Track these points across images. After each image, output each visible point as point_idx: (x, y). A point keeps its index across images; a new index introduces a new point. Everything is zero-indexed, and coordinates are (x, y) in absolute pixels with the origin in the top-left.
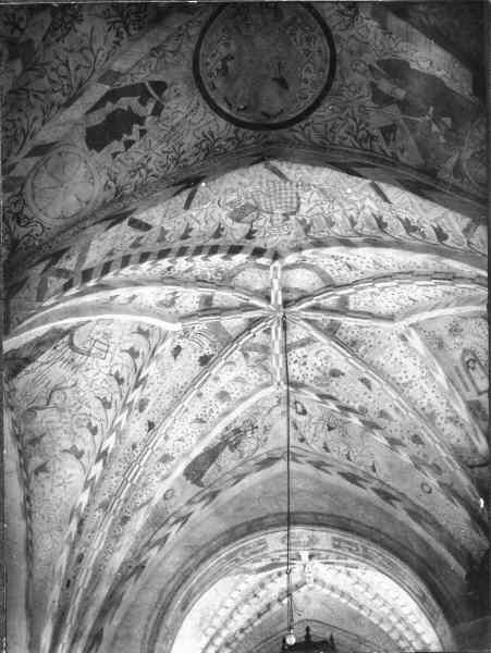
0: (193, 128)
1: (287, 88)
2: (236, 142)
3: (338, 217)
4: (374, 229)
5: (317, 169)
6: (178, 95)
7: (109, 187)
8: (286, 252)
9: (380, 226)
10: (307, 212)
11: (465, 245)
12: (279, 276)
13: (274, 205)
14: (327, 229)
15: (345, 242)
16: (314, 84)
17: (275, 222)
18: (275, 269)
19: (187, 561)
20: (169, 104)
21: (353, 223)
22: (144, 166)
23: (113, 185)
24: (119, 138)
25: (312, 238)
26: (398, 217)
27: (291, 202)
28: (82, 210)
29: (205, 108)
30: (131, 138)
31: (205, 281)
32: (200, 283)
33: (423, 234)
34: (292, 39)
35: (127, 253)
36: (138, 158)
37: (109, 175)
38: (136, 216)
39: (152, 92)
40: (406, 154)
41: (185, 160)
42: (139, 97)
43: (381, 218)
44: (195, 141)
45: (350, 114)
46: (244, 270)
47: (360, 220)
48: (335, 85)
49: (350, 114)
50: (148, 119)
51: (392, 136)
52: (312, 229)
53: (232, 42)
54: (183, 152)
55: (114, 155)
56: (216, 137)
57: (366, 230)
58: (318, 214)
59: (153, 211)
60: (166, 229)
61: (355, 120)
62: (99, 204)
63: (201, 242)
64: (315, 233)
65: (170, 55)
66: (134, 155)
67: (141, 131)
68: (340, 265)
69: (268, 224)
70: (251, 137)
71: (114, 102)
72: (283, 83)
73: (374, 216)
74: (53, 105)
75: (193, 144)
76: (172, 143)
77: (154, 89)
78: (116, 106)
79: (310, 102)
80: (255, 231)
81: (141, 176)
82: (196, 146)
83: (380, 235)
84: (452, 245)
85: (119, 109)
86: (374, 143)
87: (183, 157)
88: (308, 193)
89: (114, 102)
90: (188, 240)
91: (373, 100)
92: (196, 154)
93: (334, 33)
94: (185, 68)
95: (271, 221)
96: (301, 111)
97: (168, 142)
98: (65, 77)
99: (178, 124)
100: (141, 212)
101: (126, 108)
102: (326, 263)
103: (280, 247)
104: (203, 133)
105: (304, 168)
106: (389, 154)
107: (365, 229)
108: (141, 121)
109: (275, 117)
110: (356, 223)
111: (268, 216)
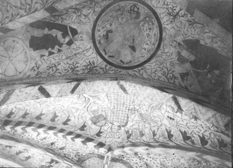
1: (135, 51)
3: (147, 131)
4: (165, 138)
5: (145, 87)
6: (82, 40)
7: (34, 70)
9: (169, 137)
10: (131, 127)
13: (115, 120)
14: (139, 138)
15: (148, 145)
16: (149, 51)
17: (113, 130)
19: (16, 17)
20: (76, 42)
21: (154, 135)
22: (55, 66)
24: (47, 49)
26: (180, 131)
27: (124, 119)
30: (53, 51)
31: (69, 158)
32: (66, 158)
33: (193, 142)
35: (34, 121)
36: (53, 61)
37: (36, 64)
38: (44, 86)
39: (70, 33)
40: (192, 87)
41: (77, 71)
42: (62, 33)
43: (170, 131)
44: (85, 64)
47: (158, 133)
48: (159, 52)
49: (165, 65)
50: (64, 46)
53: (113, 24)
54: (78, 67)
56: (95, 65)
57: (161, 140)
58: (136, 129)
60: (57, 114)
63: (72, 130)
64: (132, 139)
65: (83, 17)
66: (52, 60)
67: (59, 50)
68: (142, 163)
69: (109, 130)
71: (50, 30)
72: (133, 48)
73: (167, 130)
74: (18, 14)
78: (50, 32)
79: (146, 58)
80: (102, 132)
82: (85, 66)
83: (169, 142)
84: (211, 148)
89: (50, 29)
90: (67, 126)
92: (84, 70)
93: (163, 26)
94: (88, 28)
97: (71, 59)
98: (29, 5)
99: (78, 53)
100: (47, 85)
101: (54, 35)
102: (135, 161)
104: (90, 61)
108: (60, 45)
110: (156, 135)
111: (110, 125)
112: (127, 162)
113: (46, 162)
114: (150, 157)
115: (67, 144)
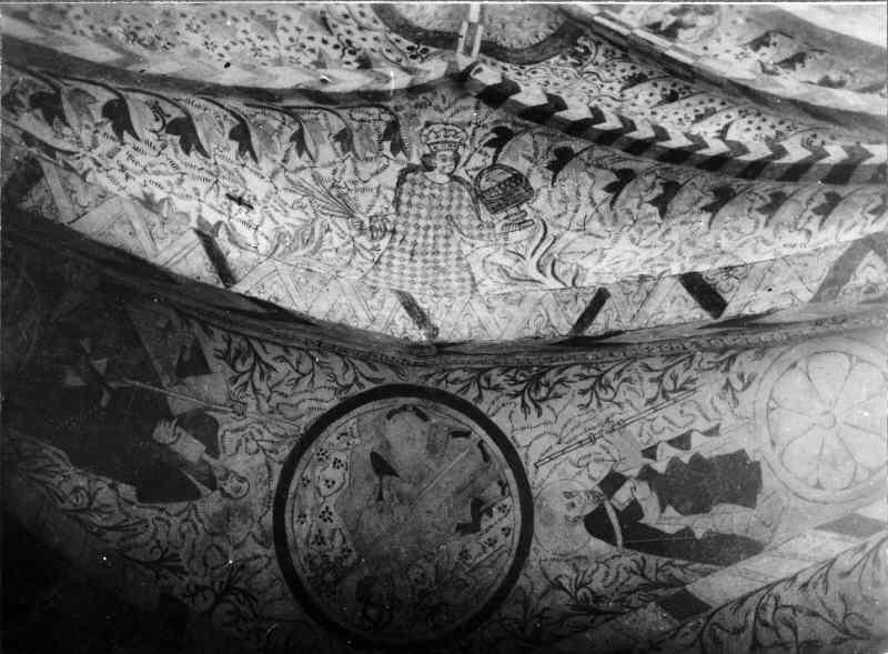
0: (556, 429)
1: (374, 455)
2: (484, 383)
3: (327, 152)
4: (257, 125)
6: (568, 495)
7: (741, 377)
8: (444, 83)
11: (65, 89)
12: (465, 25)
13: (445, 194)
14: (355, 125)
15: (321, 99)
17: (449, 154)
18: (468, 51)
19: (850, 194)
21: (299, 139)
22: (664, 393)
23: (733, 377)
24: (697, 460)
25: (387, 109)
26: (206, 155)
27: (412, 193)
28: (809, 357)
29: (527, 456)
30: (673, 452)
32: (623, 42)
34: (349, 544)
38: (707, 317)
41: (584, 378)
43: (241, 151)
44: (557, 404)
45: (263, 402)
46: (535, 47)
47: (283, 144)
48: (285, 451)
49: (263, 402)
50: (635, 472)
51: (186, 357)
52: (383, 129)
54: (583, 392)
55: (712, 432)
56: (519, 400)
59: (669, 316)
61: (255, 390)
62: (775, 352)
64: (377, 119)
65: (565, 582)
66: (679, 420)
67: (653, 457)
70: (455, 382)
75: (563, 401)
76: (602, 416)
77: (614, 534)
78: (686, 521)
80: (489, 144)
81: (674, 379)
82: (558, 396)
83: (245, 110)
85: (685, 513)
86: (223, 346)
87: (586, 384)
88: (376, 210)
91: (215, 425)
93: (271, 551)
95: (457, 159)
96: (358, 410)
100: (694, 321)
101: (670, 510)
103: (450, 98)
104: (540, 414)
105: (361, 321)
106: (196, 325)
107: (275, 124)
109: (404, 408)
110: (292, 139)
111: (461, 173)
112: (397, 32)
113: (693, 26)
114: (313, 51)
115: (616, 94)
